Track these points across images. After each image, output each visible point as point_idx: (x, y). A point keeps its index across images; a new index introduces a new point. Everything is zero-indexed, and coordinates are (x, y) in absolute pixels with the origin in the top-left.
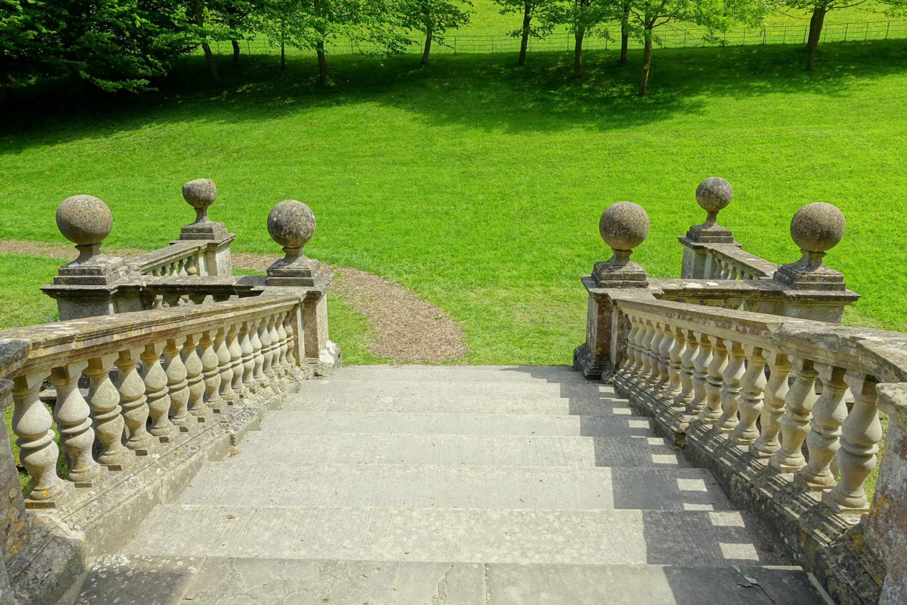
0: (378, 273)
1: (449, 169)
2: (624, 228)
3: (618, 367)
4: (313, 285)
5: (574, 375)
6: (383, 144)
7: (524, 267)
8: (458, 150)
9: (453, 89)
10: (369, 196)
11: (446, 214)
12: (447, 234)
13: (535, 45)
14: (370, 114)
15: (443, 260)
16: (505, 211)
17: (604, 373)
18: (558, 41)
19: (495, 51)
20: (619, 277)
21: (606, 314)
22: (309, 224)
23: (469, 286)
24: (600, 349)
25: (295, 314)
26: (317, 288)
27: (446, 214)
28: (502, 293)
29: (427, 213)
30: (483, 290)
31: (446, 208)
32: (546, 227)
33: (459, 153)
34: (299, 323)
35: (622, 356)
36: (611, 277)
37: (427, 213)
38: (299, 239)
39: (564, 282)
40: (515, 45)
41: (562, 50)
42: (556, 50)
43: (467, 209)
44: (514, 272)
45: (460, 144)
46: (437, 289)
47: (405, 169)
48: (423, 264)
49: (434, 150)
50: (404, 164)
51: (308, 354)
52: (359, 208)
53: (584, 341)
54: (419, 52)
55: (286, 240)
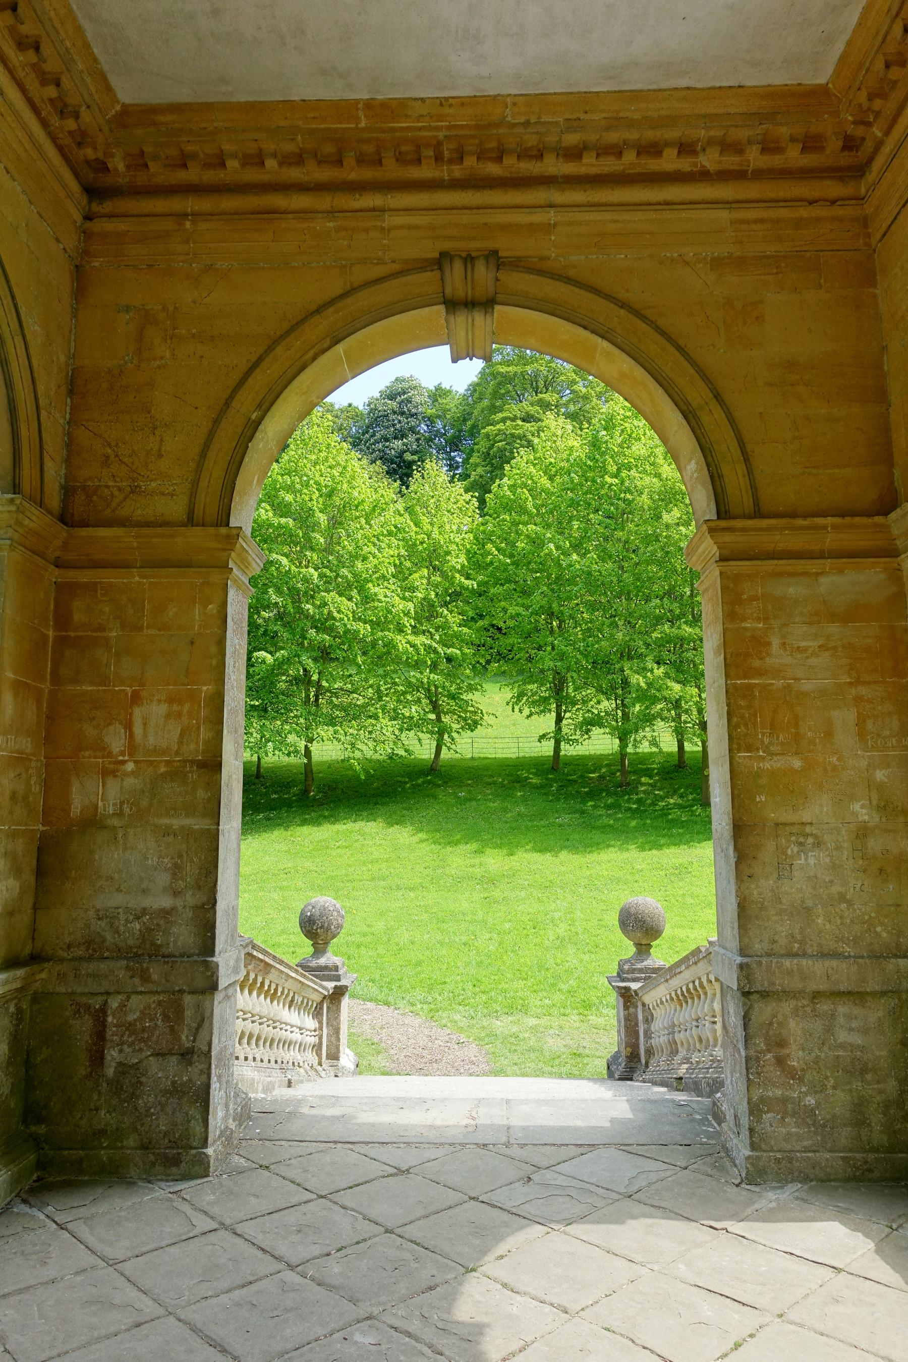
0: (387, 1004)
1: (467, 894)
2: (640, 921)
3: (647, 1066)
4: (339, 980)
5: (610, 1083)
6: (384, 865)
7: (558, 997)
8: (478, 871)
9: (470, 800)
10: (369, 926)
11: (465, 944)
12: (467, 964)
13: (567, 750)
14: (367, 830)
15: (464, 990)
16: (538, 940)
17: (635, 1075)
18: (600, 742)
19: (521, 755)
20: (641, 971)
21: (632, 1010)
22: (340, 919)
23: (496, 1014)
24: (629, 1049)
25: (322, 1008)
27: (465, 944)
28: (532, 1022)
30: (510, 1018)
31: (464, 938)
32: (586, 957)
33: (479, 876)
35: (650, 1052)
36: (633, 971)
37: (441, 943)
38: (329, 934)
39: (605, 1011)
40: (547, 749)
41: (606, 752)
42: (598, 753)
43: (491, 939)
44: (547, 1001)
46: (457, 1017)
47: (412, 894)
48: (440, 995)
49: (448, 872)
50: (412, 889)
51: (328, 1057)
53: (616, 1049)
55: (317, 934)
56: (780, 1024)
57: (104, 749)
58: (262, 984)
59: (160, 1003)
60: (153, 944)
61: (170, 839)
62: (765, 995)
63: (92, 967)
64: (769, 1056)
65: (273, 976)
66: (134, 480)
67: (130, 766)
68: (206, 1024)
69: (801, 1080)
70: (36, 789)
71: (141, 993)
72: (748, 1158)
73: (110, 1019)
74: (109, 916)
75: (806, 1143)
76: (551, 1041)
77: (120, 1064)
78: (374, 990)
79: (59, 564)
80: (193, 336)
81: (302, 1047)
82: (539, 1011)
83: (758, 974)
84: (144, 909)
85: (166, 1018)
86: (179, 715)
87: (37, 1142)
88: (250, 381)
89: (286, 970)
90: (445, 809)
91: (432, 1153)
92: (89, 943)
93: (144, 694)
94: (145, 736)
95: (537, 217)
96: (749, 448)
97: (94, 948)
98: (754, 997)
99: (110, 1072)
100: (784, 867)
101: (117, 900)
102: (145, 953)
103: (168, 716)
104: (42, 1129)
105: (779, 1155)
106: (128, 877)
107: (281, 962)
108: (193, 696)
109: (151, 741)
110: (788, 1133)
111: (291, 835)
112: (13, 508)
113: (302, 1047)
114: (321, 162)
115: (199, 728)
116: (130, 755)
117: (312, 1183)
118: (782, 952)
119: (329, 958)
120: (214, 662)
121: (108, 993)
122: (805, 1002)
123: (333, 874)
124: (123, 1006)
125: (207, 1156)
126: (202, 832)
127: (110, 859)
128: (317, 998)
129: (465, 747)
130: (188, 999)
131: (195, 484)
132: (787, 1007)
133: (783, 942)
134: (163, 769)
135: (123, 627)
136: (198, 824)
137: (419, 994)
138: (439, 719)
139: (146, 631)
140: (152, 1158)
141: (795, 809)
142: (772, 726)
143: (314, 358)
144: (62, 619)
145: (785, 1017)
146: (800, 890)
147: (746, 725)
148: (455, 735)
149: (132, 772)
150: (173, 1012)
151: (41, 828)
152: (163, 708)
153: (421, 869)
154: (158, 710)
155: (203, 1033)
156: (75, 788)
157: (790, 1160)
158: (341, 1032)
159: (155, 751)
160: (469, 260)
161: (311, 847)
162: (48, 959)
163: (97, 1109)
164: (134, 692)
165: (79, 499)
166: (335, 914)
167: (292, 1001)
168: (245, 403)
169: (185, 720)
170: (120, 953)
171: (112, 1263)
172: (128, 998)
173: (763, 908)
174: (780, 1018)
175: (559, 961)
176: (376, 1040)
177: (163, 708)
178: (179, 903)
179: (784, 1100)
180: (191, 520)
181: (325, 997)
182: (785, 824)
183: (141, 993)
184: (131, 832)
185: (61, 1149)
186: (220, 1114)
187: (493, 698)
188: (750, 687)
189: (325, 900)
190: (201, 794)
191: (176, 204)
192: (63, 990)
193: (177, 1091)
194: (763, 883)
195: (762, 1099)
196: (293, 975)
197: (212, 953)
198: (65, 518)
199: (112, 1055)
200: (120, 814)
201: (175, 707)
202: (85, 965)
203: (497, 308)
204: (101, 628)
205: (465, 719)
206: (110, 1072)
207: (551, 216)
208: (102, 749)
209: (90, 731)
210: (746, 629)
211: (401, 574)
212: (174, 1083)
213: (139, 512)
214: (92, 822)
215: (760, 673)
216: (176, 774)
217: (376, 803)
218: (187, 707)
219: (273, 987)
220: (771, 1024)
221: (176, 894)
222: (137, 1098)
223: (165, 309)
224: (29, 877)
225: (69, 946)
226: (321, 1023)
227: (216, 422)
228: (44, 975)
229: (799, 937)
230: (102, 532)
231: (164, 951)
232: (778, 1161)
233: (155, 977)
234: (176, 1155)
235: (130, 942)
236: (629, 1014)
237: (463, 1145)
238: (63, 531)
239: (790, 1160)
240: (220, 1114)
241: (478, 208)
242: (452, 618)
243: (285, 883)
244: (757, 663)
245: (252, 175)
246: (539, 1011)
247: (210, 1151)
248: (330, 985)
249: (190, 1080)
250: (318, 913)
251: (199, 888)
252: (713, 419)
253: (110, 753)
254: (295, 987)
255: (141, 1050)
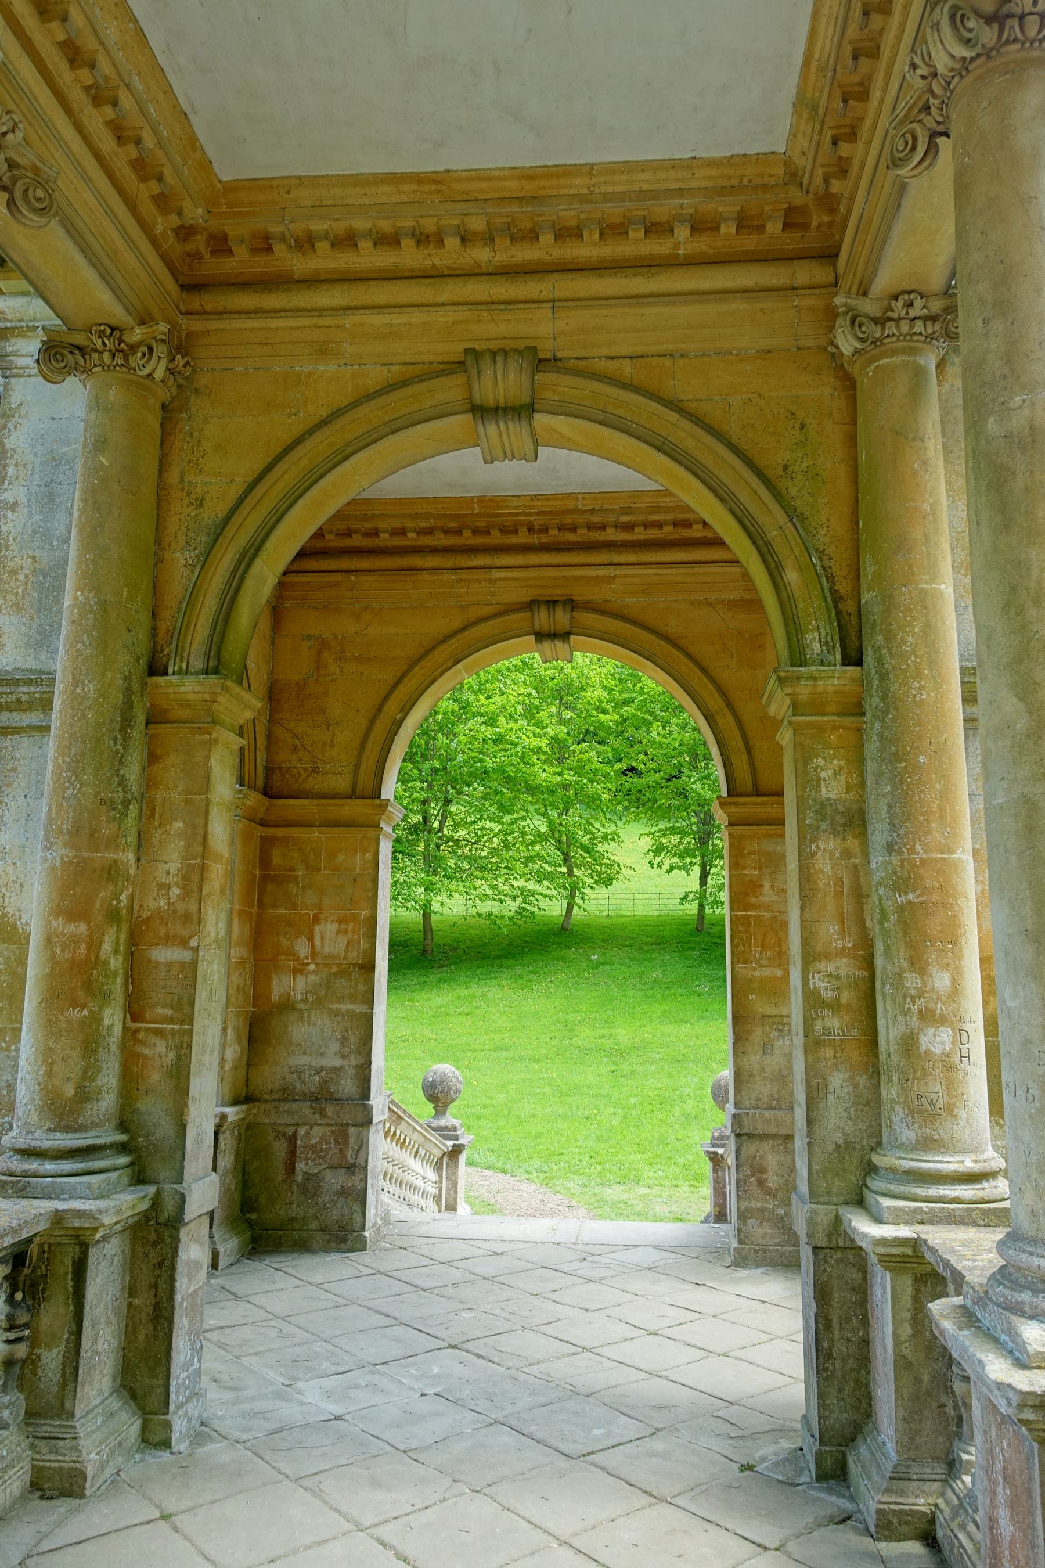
0: (505, 1172)
7: (672, 1170)
8: (607, 1043)
10: (490, 1098)
11: (587, 1118)
12: (587, 1137)
15: (580, 1161)
24: (717, 1209)
25: (441, 1164)
26: (460, 1142)
27: (587, 1118)
29: (564, 1117)
31: (587, 1112)
33: (607, 1048)
34: (444, 1172)
43: (615, 1114)
45: (611, 1035)
46: (571, 1185)
49: (574, 1043)
50: (538, 1061)
51: (447, 1209)
52: (477, 1110)
54: (558, 913)
55: (438, 1097)
56: (762, 1157)
57: (294, 954)
58: (395, 1132)
59: (333, 1132)
60: (328, 1091)
61: (340, 1019)
62: (751, 1136)
63: (287, 1106)
64: (753, 1179)
65: (403, 1126)
66: (314, 763)
67: (312, 967)
68: (364, 1147)
69: (775, 1196)
70: (249, 982)
71: (320, 1125)
72: (735, 1249)
73: (299, 1142)
74: (298, 1072)
75: (776, 1240)
76: (657, 1208)
77: (306, 1173)
78: (492, 1159)
79: (263, 824)
80: (356, 658)
81: (425, 1195)
82: (651, 1182)
83: (746, 1122)
84: (322, 1067)
85: (337, 1142)
86: (346, 932)
87: (250, 1224)
88: (396, 692)
89: (413, 1124)
90: (575, 974)
91: (520, 1246)
92: (284, 1089)
93: (322, 916)
94: (323, 946)
95: (602, 572)
96: (751, 743)
97: (287, 1094)
98: (744, 1138)
99: (299, 1178)
100: (767, 1047)
101: (301, 1060)
102: (322, 1097)
103: (338, 933)
104: (253, 1216)
105: (757, 1248)
106: (310, 1045)
107: (410, 1116)
108: (355, 919)
109: (327, 950)
110: (765, 1233)
111: (409, 1000)
112: (241, 796)
113: (425, 1195)
114: (447, 532)
115: (359, 941)
116: (312, 959)
117: (435, 1257)
118: (765, 1106)
119: (449, 1120)
120: (370, 894)
121: (298, 1124)
122: (779, 1142)
123: (454, 1043)
124: (307, 1134)
125: (365, 1237)
126: (362, 1014)
127: (298, 1031)
128: (439, 1154)
129: (597, 903)
130: (352, 1130)
131: (357, 767)
132: (766, 1145)
133: (765, 1099)
134: (334, 970)
135: (307, 868)
136: (359, 1008)
137: (536, 1163)
138: (570, 873)
139: (323, 872)
140: (328, 1237)
141: (777, 1005)
142: (762, 946)
143: (441, 675)
144: (265, 861)
145: (765, 1152)
146: (778, 1063)
147: (744, 945)
148: (587, 891)
149: (314, 971)
150: (341, 1137)
151: (252, 1009)
152: (335, 927)
153: (547, 1039)
154: (330, 928)
155: (362, 1154)
156: (275, 981)
157: (765, 1251)
158: (459, 1186)
159: (329, 956)
160: (552, 604)
161: (431, 1013)
162: (258, 1100)
163: (291, 1204)
164: (314, 915)
165: (277, 776)
166: (454, 1080)
167: (417, 1152)
168: (391, 708)
169: (350, 935)
170: (306, 1097)
171: (317, 1285)
172: (311, 1128)
173: (752, 1075)
174: (761, 1152)
175: (679, 1137)
176: (491, 1202)
177: (335, 927)
178: (345, 1063)
179: (763, 1210)
180: (353, 794)
181: (444, 1154)
182: (769, 1016)
183: (320, 1125)
184: (313, 1013)
185: (267, 1230)
186: (373, 1212)
187: (631, 844)
188: (748, 917)
189: (445, 1068)
190: (361, 987)
191: (345, 563)
192: (267, 1121)
193: (343, 1192)
194: (752, 1057)
195: (747, 1209)
196: (419, 1128)
197: (368, 1098)
198: (268, 792)
199: (300, 1167)
200: (305, 1000)
201: (343, 926)
202: (282, 1104)
203: (572, 638)
204: (292, 869)
205: (599, 875)
206: (299, 1178)
207: (612, 571)
208: (295, 956)
209: (284, 942)
210: (746, 875)
211: (530, 713)
212: (342, 1187)
213: (318, 786)
214: (287, 1006)
215: (755, 907)
216: (343, 973)
217: (501, 966)
218: (351, 925)
219: (403, 1137)
220: (755, 1157)
221: (343, 1057)
222: (318, 1196)
223: (336, 638)
224: (245, 1043)
225: (271, 1092)
226: (440, 1176)
227: (372, 722)
228: (255, 1111)
229: (776, 1096)
230: (292, 802)
231: (336, 1096)
232: (756, 1251)
233: (330, 1114)
234: (344, 1235)
235: (313, 1090)
236: (718, 1177)
237: (543, 1243)
238: (266, 801)
239: (765, 1251)
240: (373, 1212)
241: (559, 566)
242: (591, 754)
243: (403, 1052)
244: (753, 900)
245: (397, 542)
246: (651, 1182)
247: (367, 1234)
248: (450, 1143)
249: (353, 1185)
250: (439, 1079)
251: (360, 1053)
252: (726, 721)
253: (299, 957)
254: (421, 1139)
255: (320, 1164)
